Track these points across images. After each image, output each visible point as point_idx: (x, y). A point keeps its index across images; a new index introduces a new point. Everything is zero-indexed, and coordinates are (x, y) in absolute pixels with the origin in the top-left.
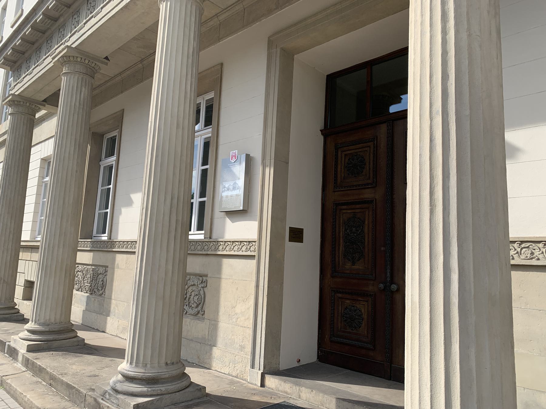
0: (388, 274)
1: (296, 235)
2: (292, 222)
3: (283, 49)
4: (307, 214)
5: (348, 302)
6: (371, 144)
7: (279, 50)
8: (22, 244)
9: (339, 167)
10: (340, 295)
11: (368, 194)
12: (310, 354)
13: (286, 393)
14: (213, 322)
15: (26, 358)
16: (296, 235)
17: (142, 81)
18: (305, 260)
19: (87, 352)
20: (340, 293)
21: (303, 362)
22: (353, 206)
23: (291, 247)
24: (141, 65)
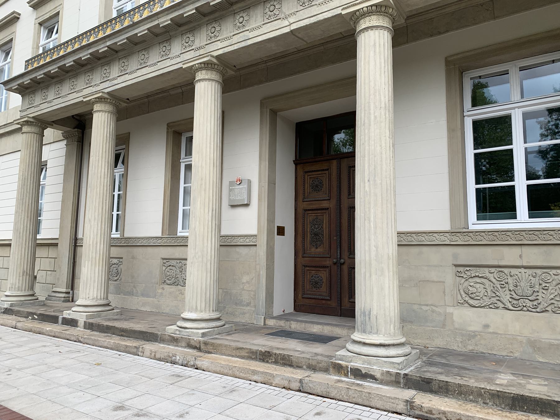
0: (339, 254)
1: (281, 231)
2: (279, 223)
3: (270, 109)
4: (286, 218)
5: (314, 272)
6: (327, 172)
7: (268, 110)
8: (38, 242)
9: (306, 185)
10: (308, 268)
11: (325, 204)
12: (290, 308)
13: (281, 326)
14: (225, 290)
15: (89, 323)
16: (281, 231)
17: (148, 112)
18: (285, 247)
19: (346, 254)
20: (308, 266)
21: (286, 312)
22: (316, 212)
23: (278, 238)
24: (146, 100)
